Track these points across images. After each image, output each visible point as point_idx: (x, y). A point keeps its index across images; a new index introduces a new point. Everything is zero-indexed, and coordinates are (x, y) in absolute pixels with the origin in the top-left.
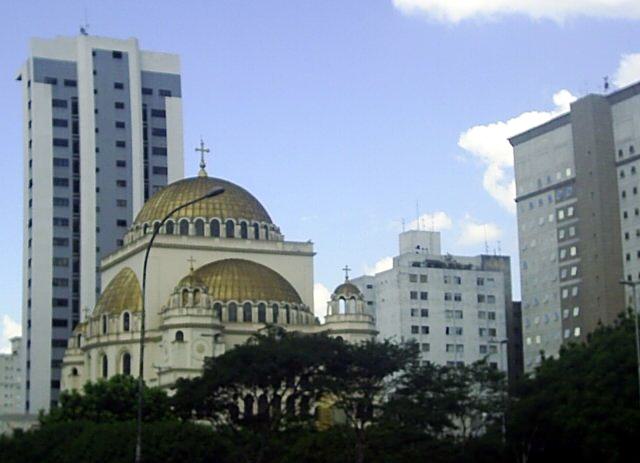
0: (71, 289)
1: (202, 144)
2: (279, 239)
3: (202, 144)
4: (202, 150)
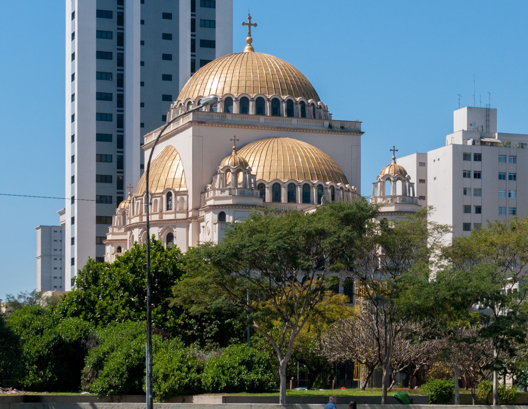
0: (115, 164)
1: (250, 18)
2: (328, 117)
3: (250, 18)
4: (250, 25)
